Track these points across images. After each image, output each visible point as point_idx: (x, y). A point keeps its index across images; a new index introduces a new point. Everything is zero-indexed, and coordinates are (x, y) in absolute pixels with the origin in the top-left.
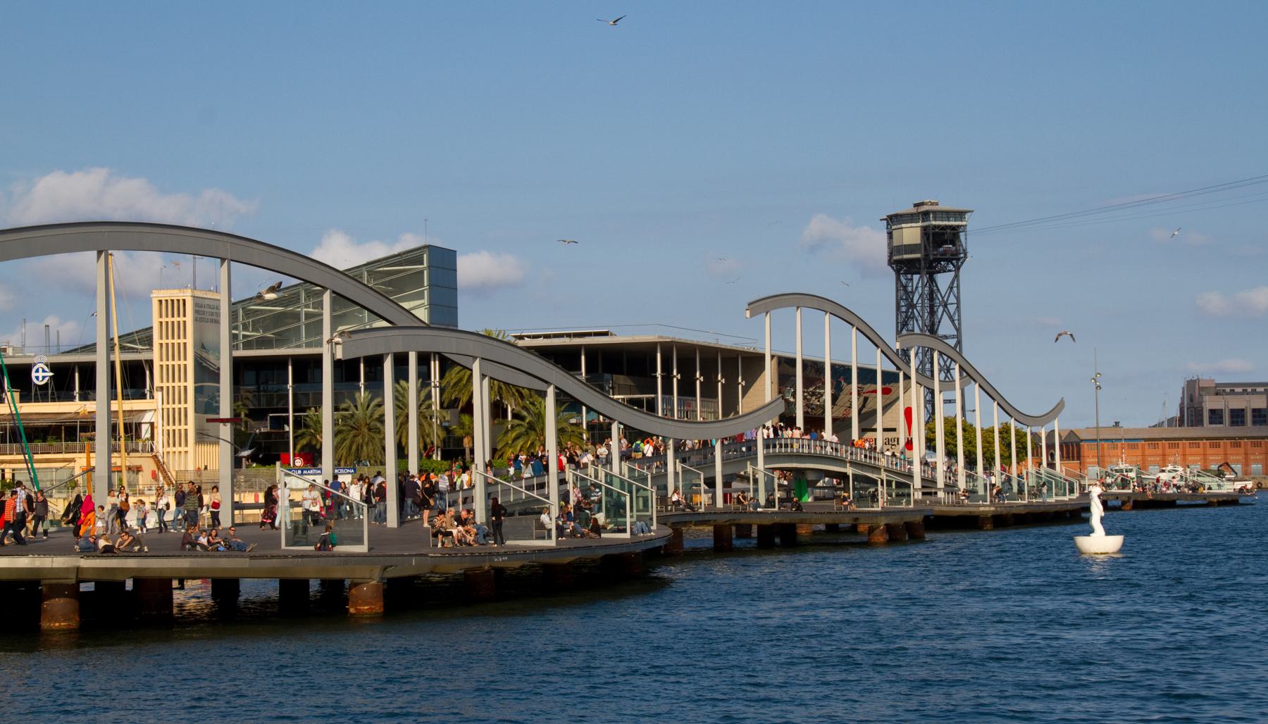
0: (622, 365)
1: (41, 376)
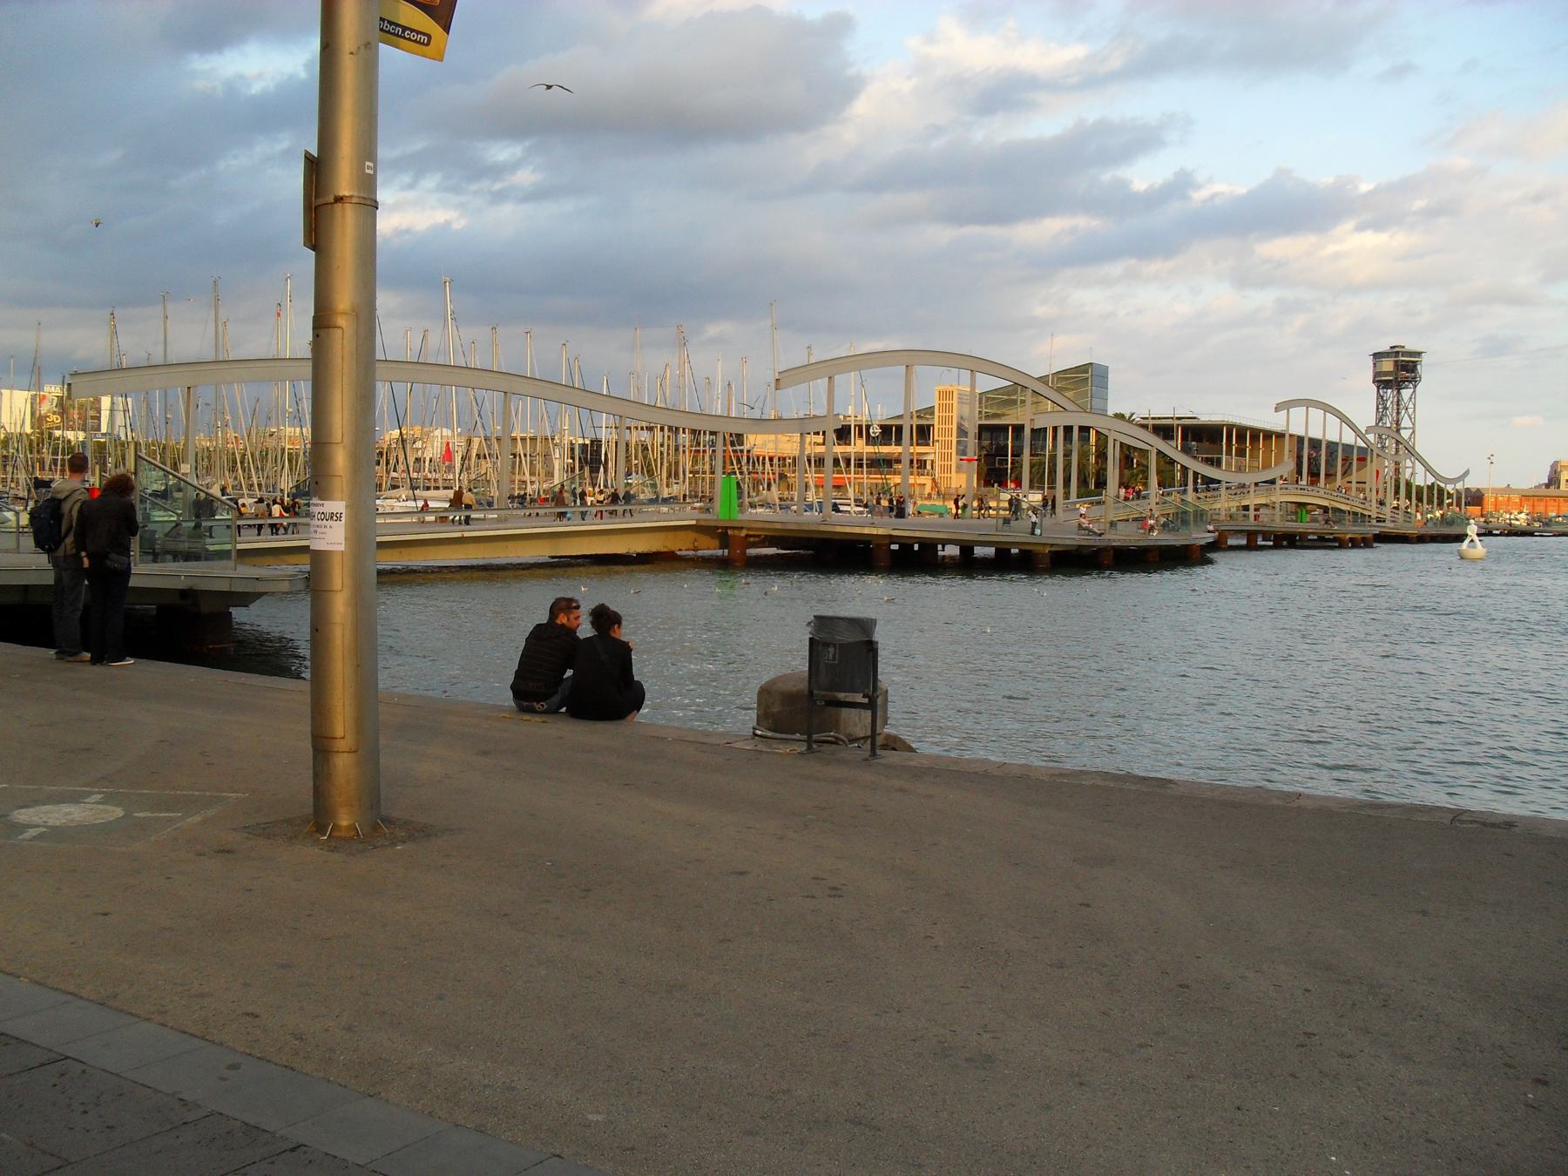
0: (1204, 437)
1: (875, 431)
